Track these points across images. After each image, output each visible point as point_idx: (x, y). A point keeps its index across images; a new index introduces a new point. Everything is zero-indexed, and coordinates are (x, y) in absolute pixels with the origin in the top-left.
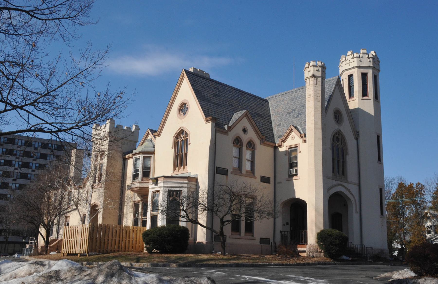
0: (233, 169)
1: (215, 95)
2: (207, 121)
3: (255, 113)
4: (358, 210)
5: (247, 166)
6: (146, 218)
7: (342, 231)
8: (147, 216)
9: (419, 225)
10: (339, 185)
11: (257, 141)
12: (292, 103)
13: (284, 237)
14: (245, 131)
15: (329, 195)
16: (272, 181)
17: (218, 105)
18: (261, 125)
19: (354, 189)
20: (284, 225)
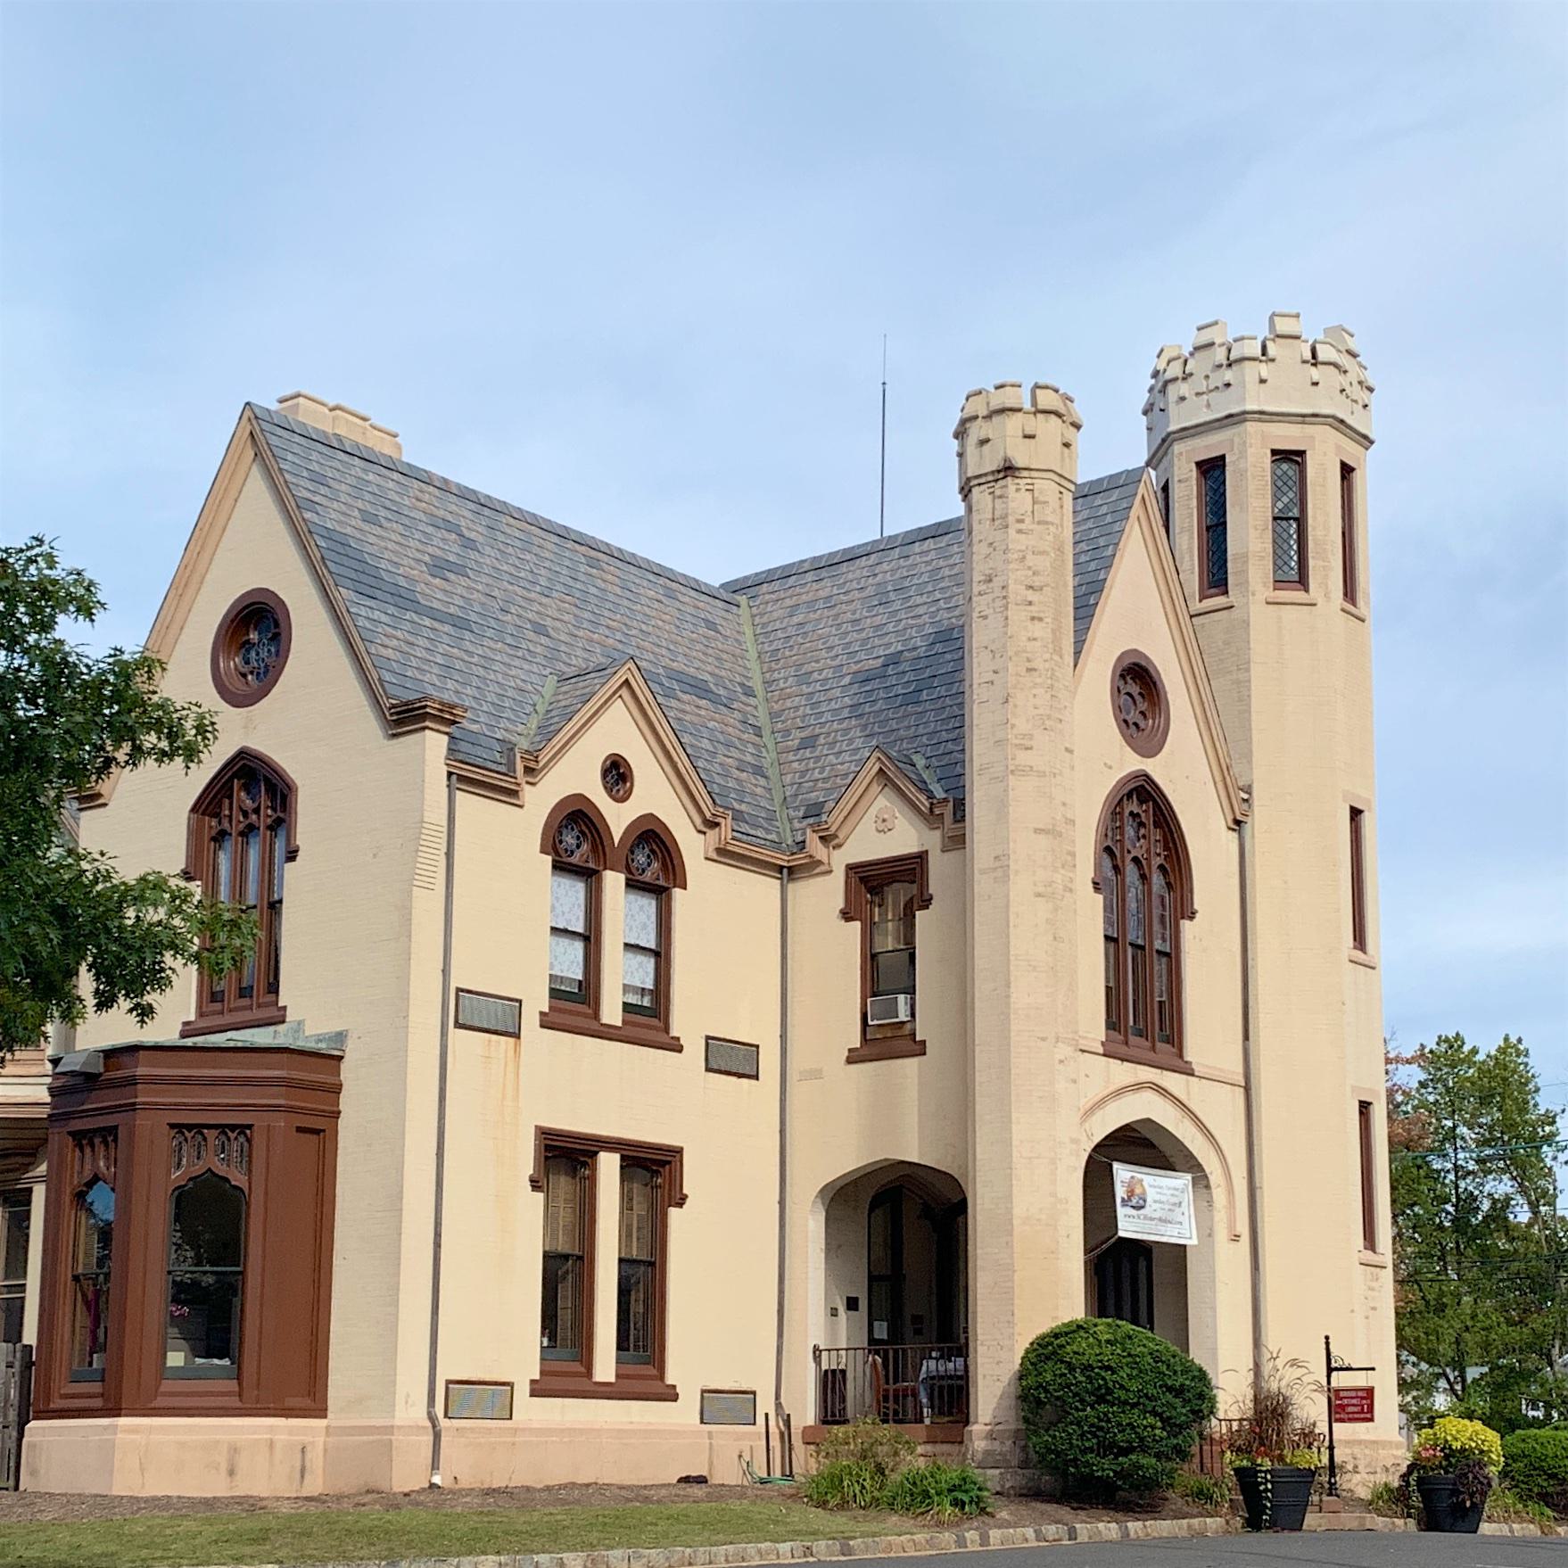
0: (555, 994)
1: (439, 567)
2: (719, 851)
3: (679, 677)
4: (1243, 1229)
5: (622, 976)
6: (22, 1287)
7: (1152, 1329)
8: (24, 1275)
9: (835, 836)
10: (1138, 1087)
11: (691, 845)
12: (878, 620)
13: (831, 1383)
14: (617, 774)
15: (1090, 1146)
16: (769, 1062)
17: (461, 624)
18: (706, 744)
19: (1220, 1108)
20: (834, 1312)
